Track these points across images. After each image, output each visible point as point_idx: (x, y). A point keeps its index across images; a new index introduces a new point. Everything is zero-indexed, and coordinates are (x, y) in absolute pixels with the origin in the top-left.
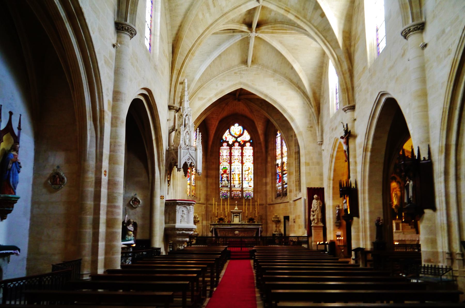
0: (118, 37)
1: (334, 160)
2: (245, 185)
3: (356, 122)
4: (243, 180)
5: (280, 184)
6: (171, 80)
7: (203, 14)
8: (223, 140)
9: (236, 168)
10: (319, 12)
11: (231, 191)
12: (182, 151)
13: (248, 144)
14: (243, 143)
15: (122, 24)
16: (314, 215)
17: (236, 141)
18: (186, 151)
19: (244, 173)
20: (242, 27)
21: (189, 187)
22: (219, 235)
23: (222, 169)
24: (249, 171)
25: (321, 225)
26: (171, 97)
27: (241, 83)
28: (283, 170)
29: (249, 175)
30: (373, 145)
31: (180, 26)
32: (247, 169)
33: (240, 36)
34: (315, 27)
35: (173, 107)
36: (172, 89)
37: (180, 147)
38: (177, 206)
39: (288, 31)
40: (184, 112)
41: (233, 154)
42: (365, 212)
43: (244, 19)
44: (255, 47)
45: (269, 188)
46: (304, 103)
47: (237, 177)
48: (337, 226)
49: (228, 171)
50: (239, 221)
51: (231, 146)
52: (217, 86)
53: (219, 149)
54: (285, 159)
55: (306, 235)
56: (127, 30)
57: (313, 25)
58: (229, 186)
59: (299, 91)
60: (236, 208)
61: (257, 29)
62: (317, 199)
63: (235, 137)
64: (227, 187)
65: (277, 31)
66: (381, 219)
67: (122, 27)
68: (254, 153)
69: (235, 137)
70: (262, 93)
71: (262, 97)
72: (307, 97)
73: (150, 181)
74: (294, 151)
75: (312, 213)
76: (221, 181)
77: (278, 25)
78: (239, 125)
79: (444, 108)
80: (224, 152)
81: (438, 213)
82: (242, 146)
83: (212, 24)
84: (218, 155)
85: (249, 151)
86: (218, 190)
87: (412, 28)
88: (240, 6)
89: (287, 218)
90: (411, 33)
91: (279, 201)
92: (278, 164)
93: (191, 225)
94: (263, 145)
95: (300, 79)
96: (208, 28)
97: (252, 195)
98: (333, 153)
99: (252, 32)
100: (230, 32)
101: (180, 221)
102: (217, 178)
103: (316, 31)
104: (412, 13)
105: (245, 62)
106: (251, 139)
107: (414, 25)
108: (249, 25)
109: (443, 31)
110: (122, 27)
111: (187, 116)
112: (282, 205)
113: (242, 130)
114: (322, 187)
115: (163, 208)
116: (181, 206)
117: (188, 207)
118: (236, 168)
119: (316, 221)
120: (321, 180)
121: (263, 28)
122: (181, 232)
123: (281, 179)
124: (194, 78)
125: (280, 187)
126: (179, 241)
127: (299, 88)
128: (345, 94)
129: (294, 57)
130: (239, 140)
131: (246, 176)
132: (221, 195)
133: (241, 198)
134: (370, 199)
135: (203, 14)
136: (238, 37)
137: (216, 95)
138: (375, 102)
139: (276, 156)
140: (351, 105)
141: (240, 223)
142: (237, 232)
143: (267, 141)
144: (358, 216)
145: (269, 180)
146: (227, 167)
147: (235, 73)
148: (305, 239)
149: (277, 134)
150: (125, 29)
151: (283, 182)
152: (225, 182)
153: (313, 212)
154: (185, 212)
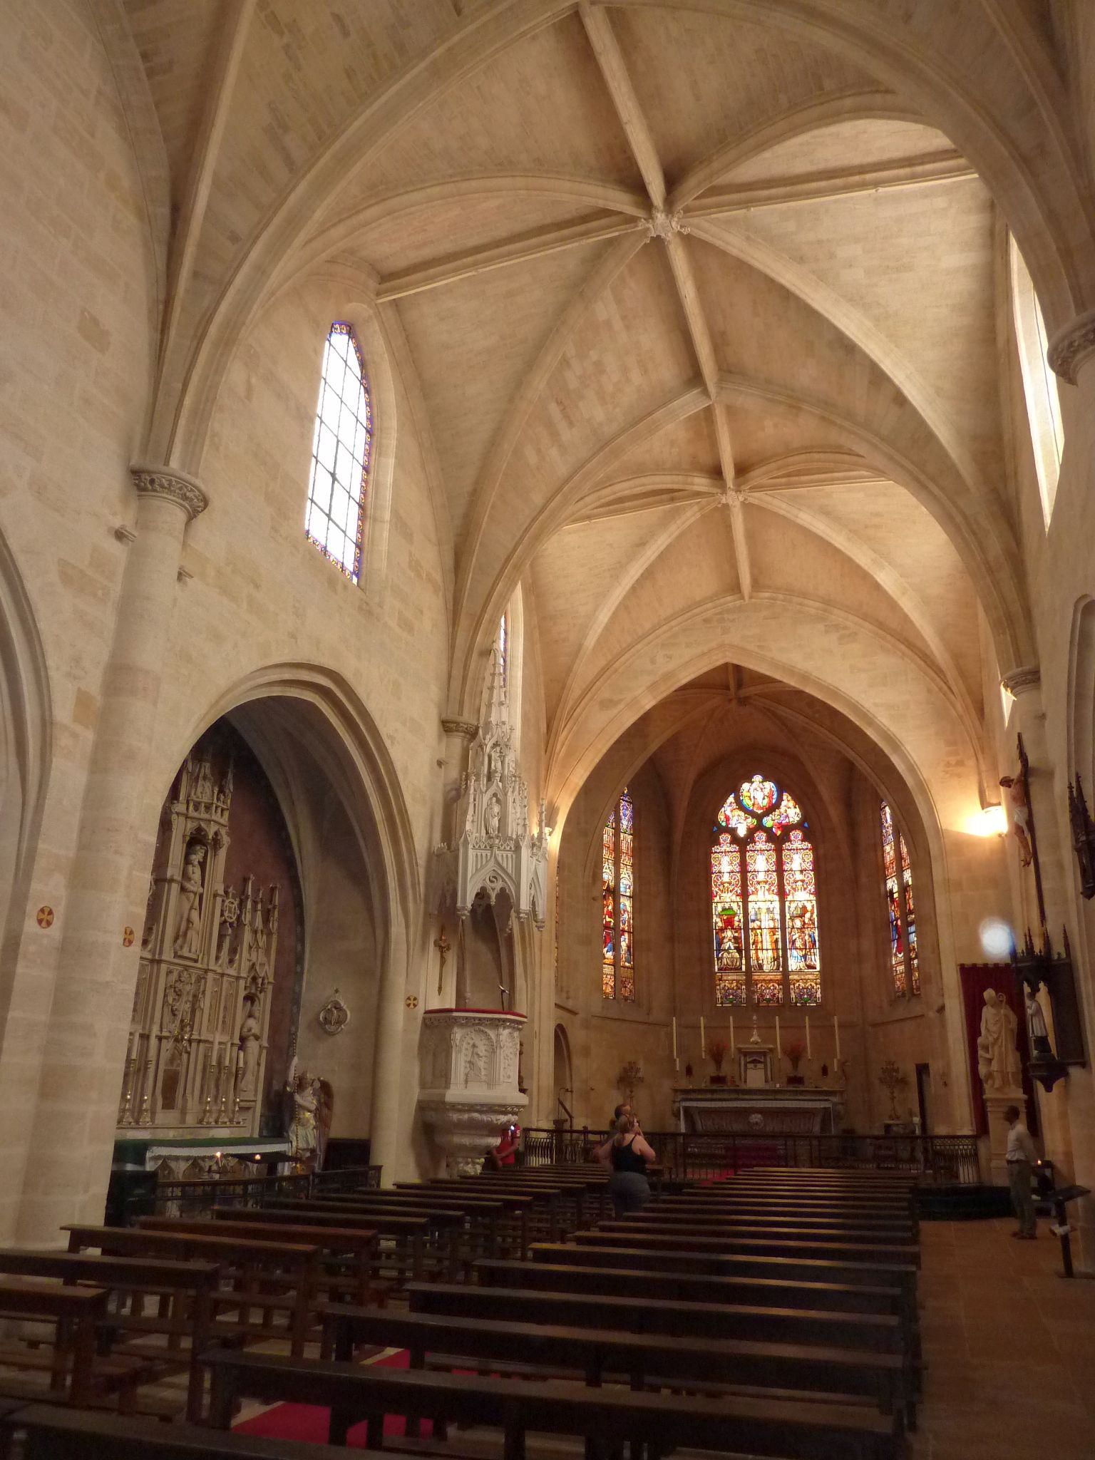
2: (794, 963)
6: (452, 647)
7: (539, 451)
8: (716, 823)
11: (749, 982)
12: (471, 853)
13: (796, 835)
14: (779, 833)
15: (149, 472)
16: (990, 1061)
17: (760, 827)
19: (789, 923)
20: (690, 479)
21: (608, 970)
22: (699, 1127)
23: (720, 916)
28: (905, 913)
33: (696, 508)
35: (458, 723)
36: (454, 672)
38: (456, 1029)
39: (836, 475)
41: (785, 867)
44: (751, 537)
46: (929, 691)
47: (767, 942)
49: (738, 920)
51: (743, 844)
52: (653, 661)
53: (709, 853)
55: (967, 1131)
56: (169, 489)
58: (744, 968)
60: (755, 1038)
61: (741, 479)
68: (816, 862)
70: (791, 671)
71: (793, 682)
72: (939, 671)
73: (379, 951)
75: (981, 1052)
78: (765, 779)
80: (724, 863)
82: (779, 840)
84: (706, 871)
85: (799, 859)
86: (708, 979)
88: (650, 414)
90: (1080, 356)
91: (900, 1012)
92: (891, 893)
93: (507, 1092)
95: (906, 618)
97: (819, 995)
101: (462, 1077)
102: (705, 940)
105: (735, 588)
106: (805, 817)
107: (1084, 325)
110: (152, 481)
111: (498, 749)
115: (416, 1037)
117: (492, 1034)
119: (998, 1083)
121: (757, 476)
122: (466, 1116)
124: (580, 646)
125: (901, 968)
126: (462, 1148)
127: (910, 645)
129: (874, 551)
130: (768, 822)
132: (719, 996)
133: (783, 1005)
137: (653, 687)
138: (1071, 642)
139: (884, 868)
140: (1026, 668)
141: (767, 1088)
142: (756, 1118)
143: (851, 825)
146: (734, 906)
147: (706, 621)
150: (162, 486)
152: (729, 952)
153: (986, 1049)
154: (482, 1049)
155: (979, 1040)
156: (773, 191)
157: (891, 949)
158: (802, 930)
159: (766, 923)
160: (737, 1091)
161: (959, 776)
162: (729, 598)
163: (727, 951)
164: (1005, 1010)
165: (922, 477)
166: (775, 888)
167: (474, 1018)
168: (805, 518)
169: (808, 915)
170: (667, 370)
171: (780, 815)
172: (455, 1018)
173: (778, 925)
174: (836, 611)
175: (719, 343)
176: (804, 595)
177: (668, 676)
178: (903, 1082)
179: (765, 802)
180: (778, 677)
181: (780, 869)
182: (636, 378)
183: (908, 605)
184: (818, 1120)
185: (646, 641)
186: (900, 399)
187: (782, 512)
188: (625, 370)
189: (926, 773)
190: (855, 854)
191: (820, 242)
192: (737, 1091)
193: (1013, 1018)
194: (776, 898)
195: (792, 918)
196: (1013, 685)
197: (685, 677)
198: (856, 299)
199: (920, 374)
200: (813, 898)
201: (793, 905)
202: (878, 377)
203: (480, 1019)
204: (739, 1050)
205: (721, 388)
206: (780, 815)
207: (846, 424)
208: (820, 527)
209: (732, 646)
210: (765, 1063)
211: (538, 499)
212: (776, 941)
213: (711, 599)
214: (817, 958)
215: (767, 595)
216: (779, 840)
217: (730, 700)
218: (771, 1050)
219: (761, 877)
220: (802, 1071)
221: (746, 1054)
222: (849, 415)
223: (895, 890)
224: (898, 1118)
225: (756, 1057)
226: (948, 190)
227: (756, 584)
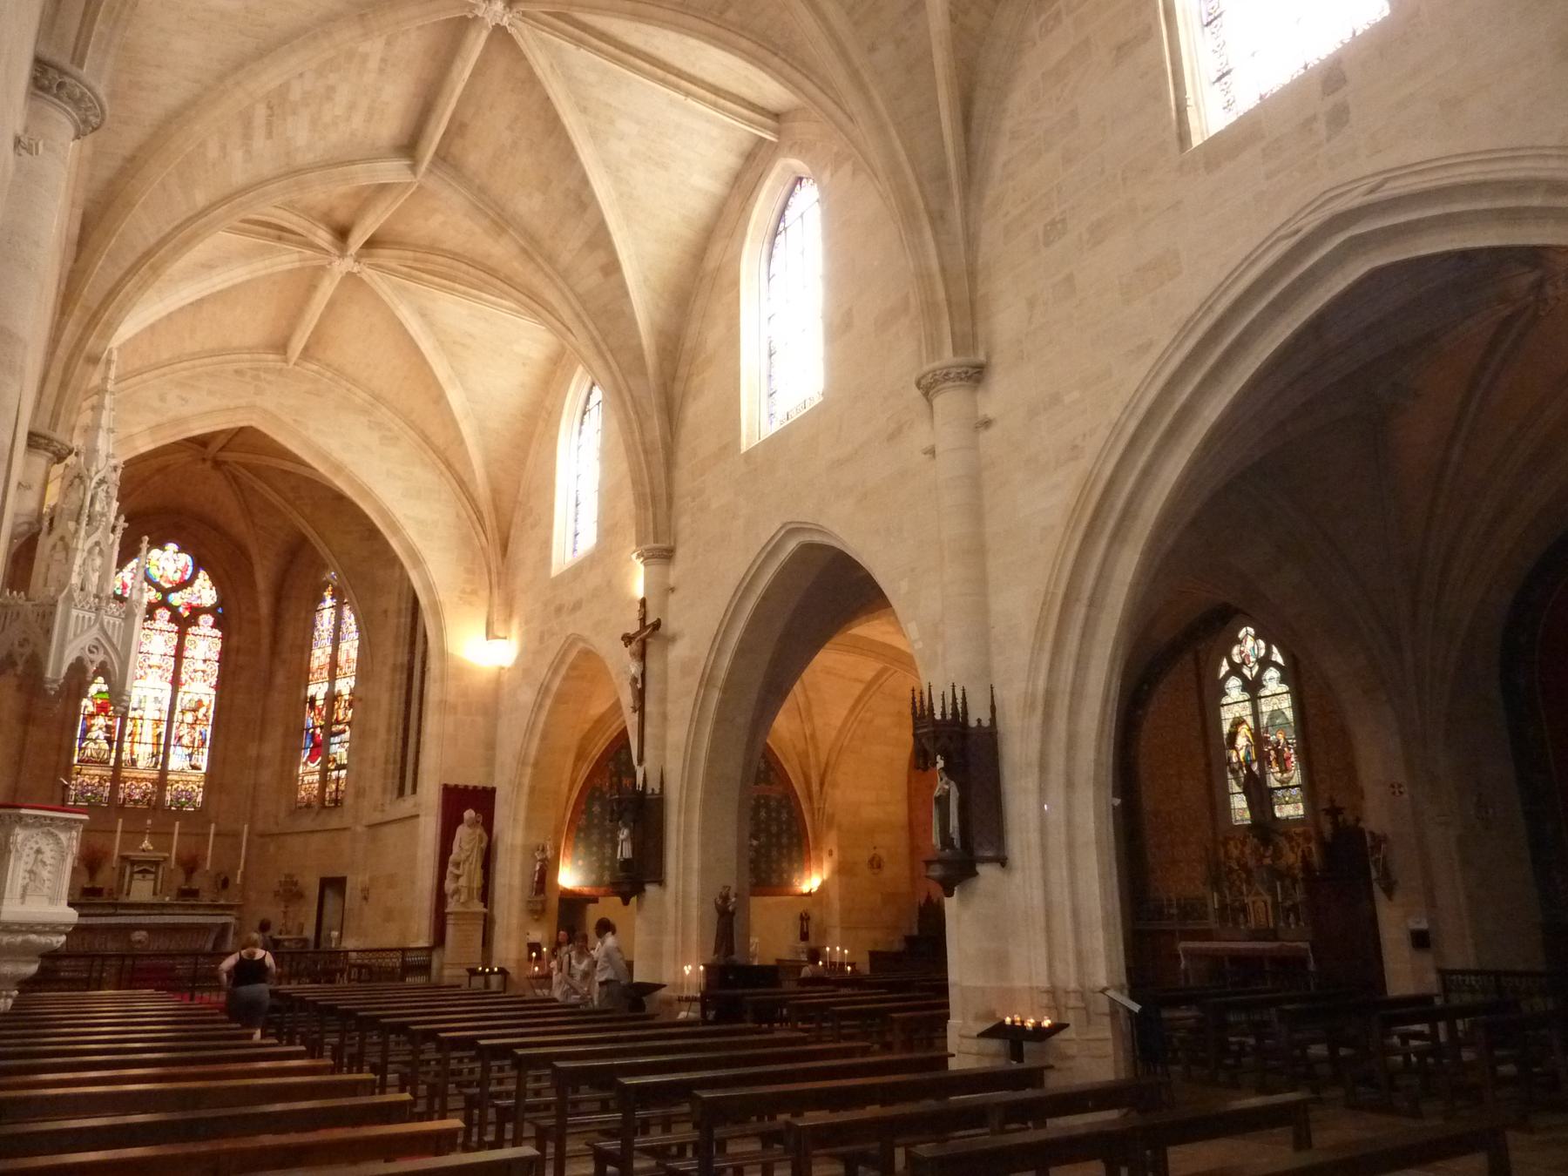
0: (34, 115)
1: (548, 702)
2: (177, 760)
3: (672, 598)
4: (173, 742)
5: (315, 766)
7: (223, 147)
9: (150, 699)
10: (601, 257)
11: (116, 779)
13: (206, 620)
14: (187, 614)
15: (62, 72)
16: (458, 877)
18: (87, 615)
19: (177, 716)
20: (314, 229)
24: (200, 714)
25: (478, 907)
26: (44, 400)
27: (251, 407)
29: (198, 728)
30: (732, 672)
31: (131, 159)
32: (193, 705)
33: (295, 256)
34: (578, 296)
37: (70, 598)
38: (18, 830)
39: (457, 286)
40: (93, 469)
41: (186, 654)
42: (687, 869)
43: (332, 209)
44: (331, 305)
45: (267, 776)
46: (458, 516)
47: (148, 734)
48: (533, 912)
50: (155, 894)
52: (162, 399)
54: (345, 686)
55: (423, 943)
56: (77, 102)
57: (572, 289)
58: (112, 762)
59: (448, 475)
60: (146, 844)
62: (473, 825)
63: (158, 588)
64: (106, 762)
65: (425, 276)
66: (732, 893)
67: (61, 86)
69: (158, 588)
70: (325, 458)
72: (472, 499)
74: (390, 661)
75: (450, 868)
76: (83, 739)
77: (440, 259)
79: (1047, 592)
81: (1018, 877)
82: (184, 622)
83: (244, 190)
85: (205, 644)
87: (953, 372)
88: (352, 162)
89: (334, 885)
90: (950, 384)
91: (307, 823)
92: (313, 700)
94: (266, 630)
96: (227, 199)
97: (199, 799)
98: (551, 680)
99: (343, 253)
100: (266, 235)
101: (19, 890)
103: (578, 307)
104: (953, 334)
106: (222, 601)
108: (342, 234)
109: (1056, 399)
110: (61, 86)
111: (104, 487)
112: (317, 837)
113: (190, 570)
114: (489, 786)
116: (34, 831)
118: (150, 699)
120: (490, 761)
121: (385, 256)
122: (20, 939)
123: (320, 748)
128: (646, 509)
130: (175, 599)
131: (184, 730)
133: (155, 808)
134: (704, 830)
135: (223, 147)
136: (285, 258)
141: (155, 900)
142: (139, 936)
143: (277, 616)
144: (660, 881)
145: (271, 748)
148: (422, 958)
149: (323, 600)
151: (326, 761)
152: (96, 741)
153: (457, 865)
155: (452, 858)
156: (604, 46)
157: (299, 757)
158: (192, 726)
159: (151, 712)
160: (115, 906)
161: (471, 604)
162: (271, 357)
163: (94, 741)
164: (479, 830)
165: (604, 347)
166: (169, 675)
167: (45, 817)
168: (405, 314)
169: (203, 710)
170: (389, 128)
171: (192, 594)
172: (21, 817)
173: (165, 717)
174: (384, 409)
175: (457, 128)
176: (355, 382)
177: (178, 421)
178: (300, 896)
179: (177, 577)
180: (315, 465)
181: (179, 655)
182: (358, 121)
183: (467, 429)
184: (213, 936)
185: (157, 372)
186: (612, 267)
187: (386, 298)
188: (352, 107)
189: (443, 596)
190: (274, 651)
191: (608, 105)
192: (115, 906)
193: (485, 838)
194: (169, 687)
195: (183, 712)
196: (650, 557)
197: (198, 429)
198: (613, 170)
199: (642, 256)
200: (213, 692)
201: (187, 697)
202: (600, 239)
203: (52, 819)
204: (124, 859)
205: (430, 171)
206: (192, 594)
207: (547, 268)
208: (414, 326)
209: (265, 411)
210: (156, 873)
211: (201, 198)
212: (159, 735)
213: (250, 350)
214: (205, 757)
215: (315, 368)
216: (184, 622)
217: (204, 460)
218: (165, 859)
219: (155, 660)
220: (198, 882)
221: (133, 863)
222: (550, 259)
223: (320, 696)
224: (288, 933)
225: (147, 867)
226: (725, 127)
227: (306, 353)
